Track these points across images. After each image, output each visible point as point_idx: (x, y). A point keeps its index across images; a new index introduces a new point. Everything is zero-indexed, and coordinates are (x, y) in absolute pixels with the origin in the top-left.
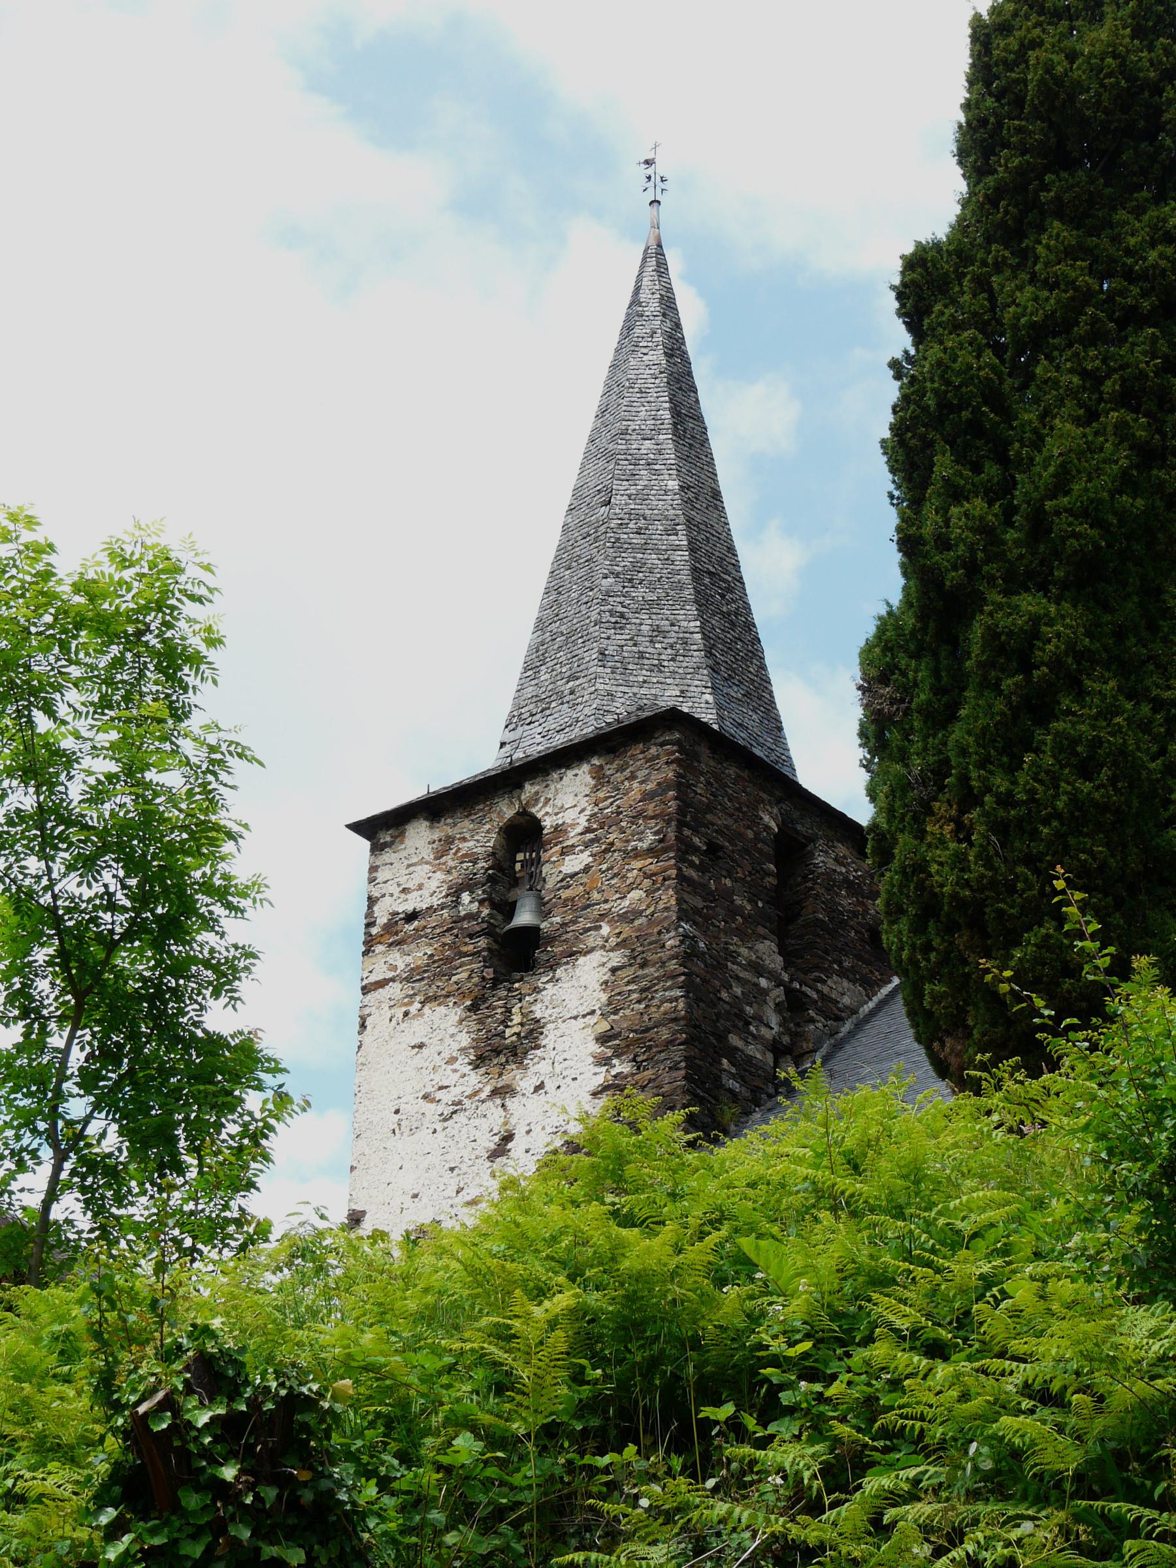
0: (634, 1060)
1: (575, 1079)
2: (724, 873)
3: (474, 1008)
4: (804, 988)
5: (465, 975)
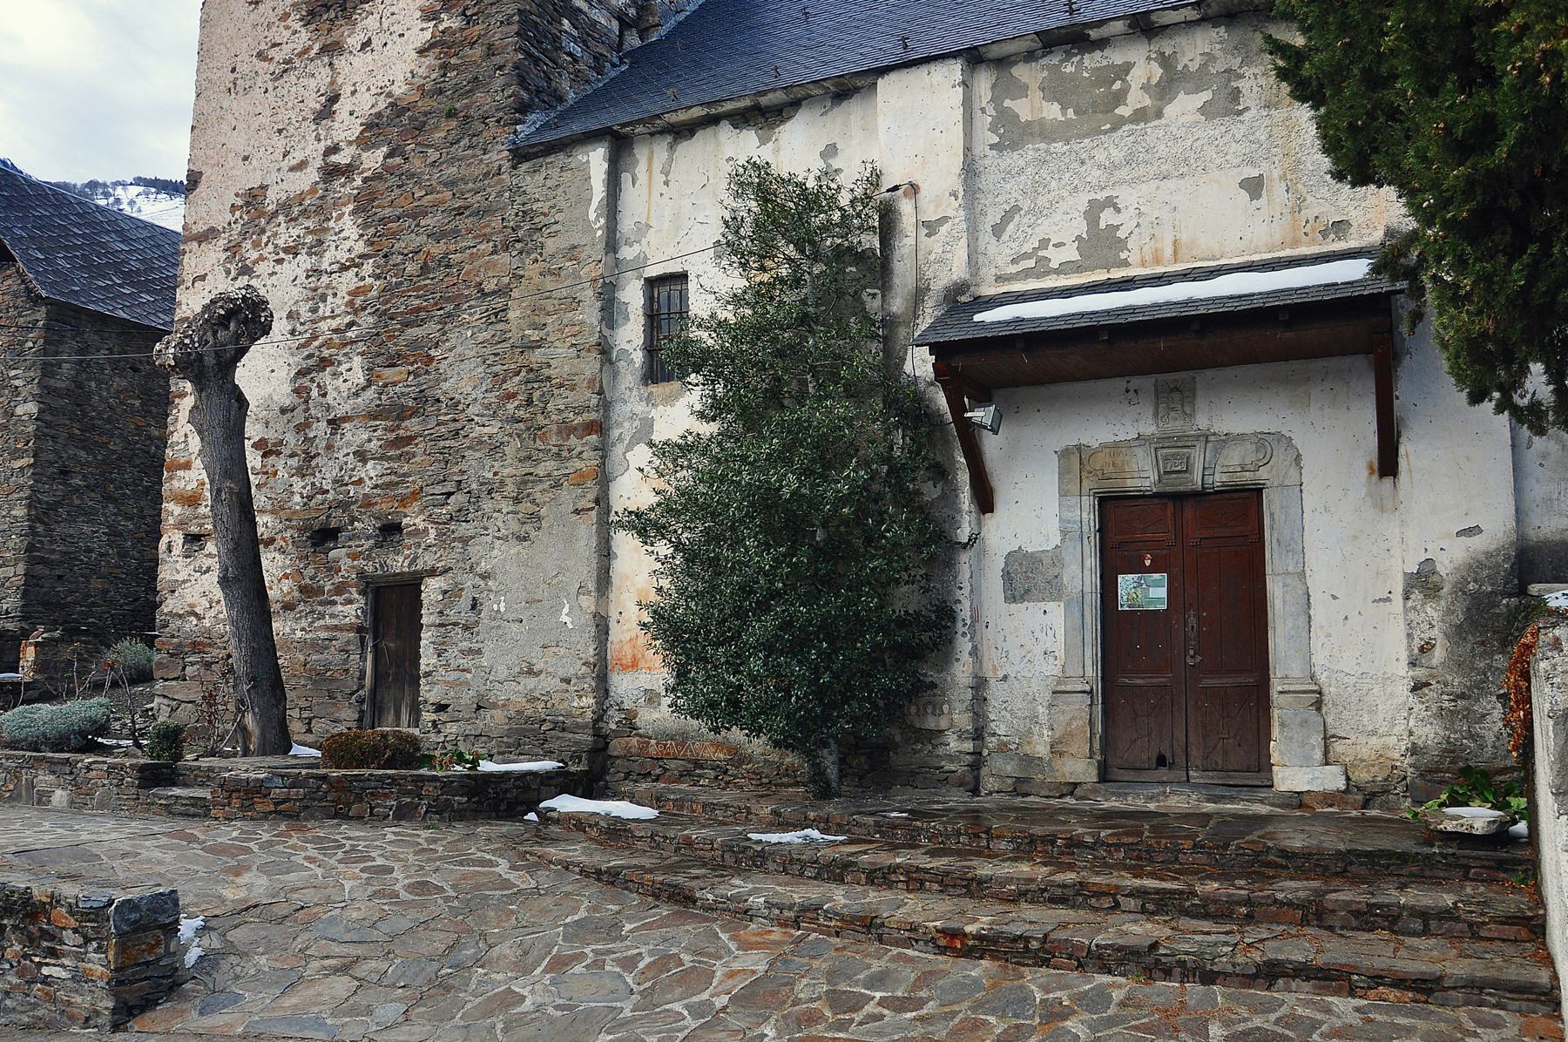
0: (464, 14)
1: (402, 35)
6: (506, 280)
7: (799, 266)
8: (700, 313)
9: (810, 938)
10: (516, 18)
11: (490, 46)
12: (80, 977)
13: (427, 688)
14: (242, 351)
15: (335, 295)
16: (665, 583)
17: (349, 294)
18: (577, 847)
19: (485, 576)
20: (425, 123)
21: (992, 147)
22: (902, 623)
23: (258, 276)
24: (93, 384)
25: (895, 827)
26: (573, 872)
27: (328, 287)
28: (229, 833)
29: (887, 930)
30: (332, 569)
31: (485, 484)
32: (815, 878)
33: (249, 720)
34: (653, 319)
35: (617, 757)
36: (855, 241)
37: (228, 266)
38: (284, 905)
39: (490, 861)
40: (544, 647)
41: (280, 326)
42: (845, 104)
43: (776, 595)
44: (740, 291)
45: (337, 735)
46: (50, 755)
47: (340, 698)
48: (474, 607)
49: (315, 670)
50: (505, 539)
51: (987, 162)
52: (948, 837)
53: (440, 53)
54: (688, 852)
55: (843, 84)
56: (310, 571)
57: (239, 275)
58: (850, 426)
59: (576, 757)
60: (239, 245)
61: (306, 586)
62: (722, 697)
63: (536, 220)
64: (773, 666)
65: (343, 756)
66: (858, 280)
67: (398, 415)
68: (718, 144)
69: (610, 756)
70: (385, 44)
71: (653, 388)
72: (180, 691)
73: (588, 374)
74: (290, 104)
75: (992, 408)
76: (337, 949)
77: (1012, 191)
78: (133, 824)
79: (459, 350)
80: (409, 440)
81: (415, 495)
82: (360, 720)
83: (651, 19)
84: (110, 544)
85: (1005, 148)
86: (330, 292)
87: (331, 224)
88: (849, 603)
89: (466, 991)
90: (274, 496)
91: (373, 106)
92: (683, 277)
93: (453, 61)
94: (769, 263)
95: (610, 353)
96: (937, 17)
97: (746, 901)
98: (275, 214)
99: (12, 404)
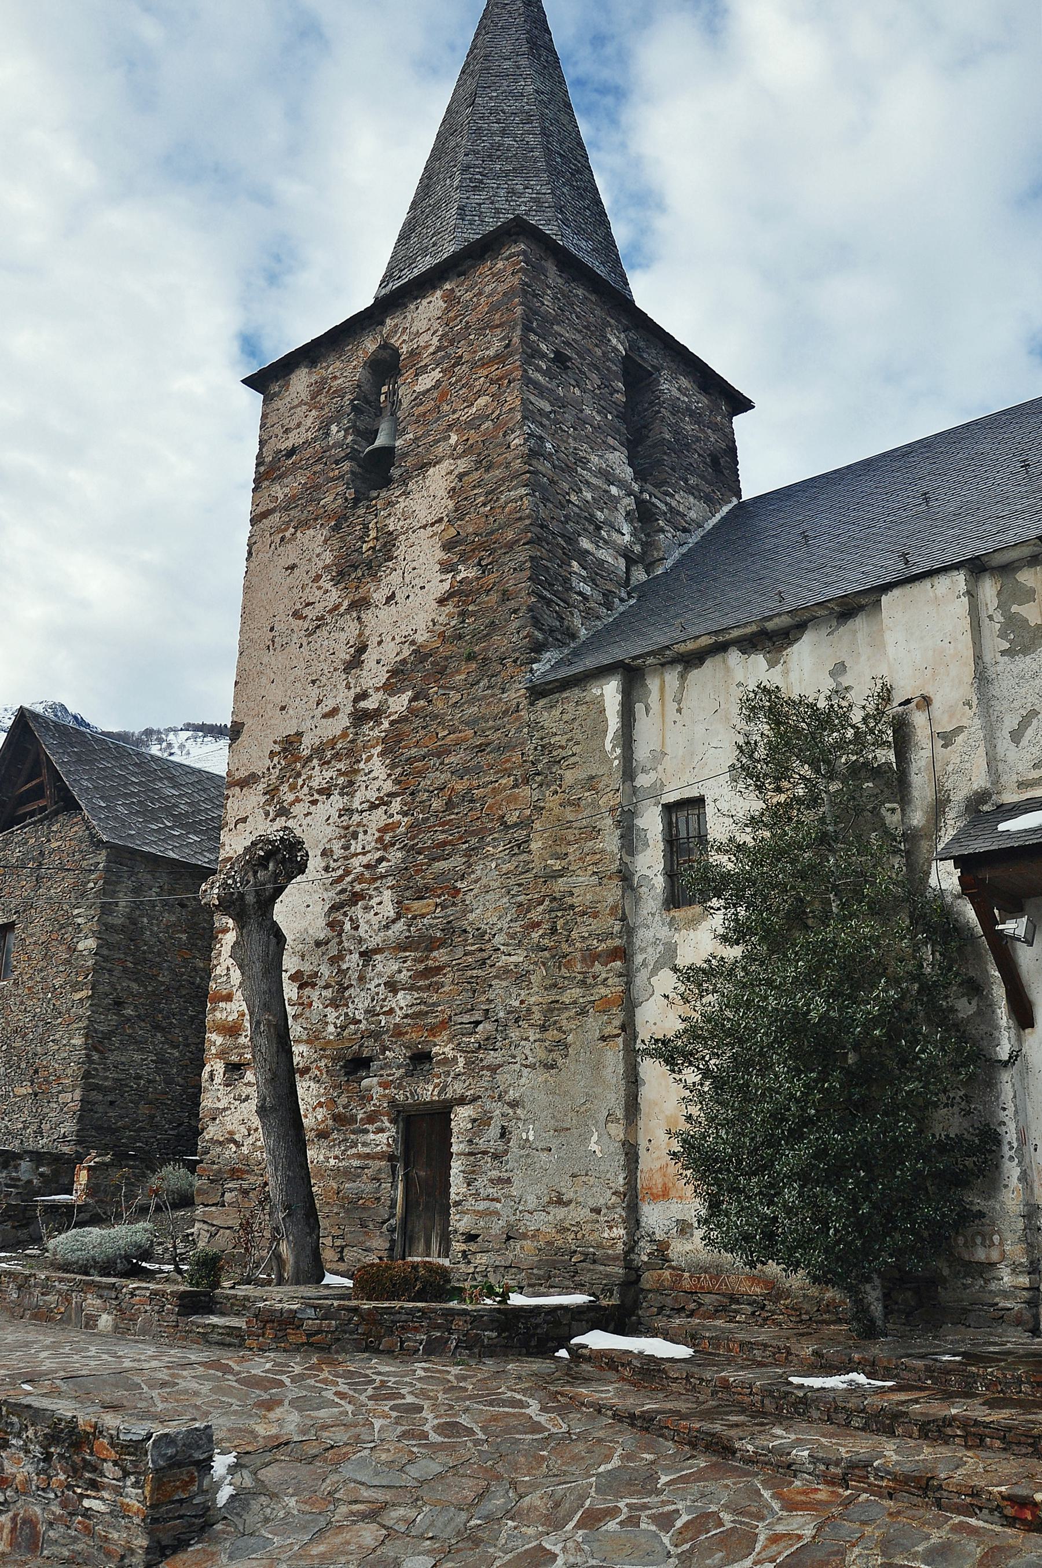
0: (479, 564)
1: (423, 588)
2: (573, 382)
3: (337, 528)
4: (654, 500)
5: (331, 498)
6: (528, 812)
7: (814, 786)
8: (718, 837)
9: (860, 1499)
10: (528, 564)
11: (505, 592)
12: (120, 1512)
13: (457, 1217)
14: (279, 891)
15: (365, 832)
16: (694, 1110)
17: (379, 830)
18: (610, 1388)
19: (514, 1104)
20: (446, 667)
21: (1003, 653)
22: (943, 1147)
23: (295, 817)
24: (145, 920)
25: (948, 1373)
26: (606, 1415)
27: (359, 825)
28: (261, 1366)
29: (945, 1494)
30: (365, 1098)
31: (512, 1012)
32: (863, 1429)
33: (284, 1248)
34: (672, 843)
35: (650, 1291)
36: (870, 757)
37: (268, 808)
38: (314, 1443)
39: (521, 1401)
40: (574, 1176)
41: (315, 863)
42: (850, 622)
43: (809, 1122)
44: (757, 813)
45: (369, 1265)
46: (98, 1279)
47: (371, 1227)
48: (503, 1135)
49: (347, 1198)
50: (532, 1067)
51: (999, 668)
52: (1008, 1385)
53: (459, 601)
54: (725, 1396)
55: (847, 604)
56: (343, 1100)
57: (277, 816)
58: (878, 946)
59: (608, 1291)
60: (277, 789)
61: (339, 1115)
62: (756, 1230)
63: (555, 753)
64: (809, 1196)
65: (374, 1288)
66: (876, 796)
67: (427, 946)
68: (728, 670)
69: (643, 1290)
70: (408, 597)
71: (675, 913)
72: (220, 1217)
73: (610, 901)
74: (322, 657)
75: (1025, 919)
76: (365, 1493)
77: (1027, 696)
78: (172, 1352)
79: (484, 881)
80: (438, 969)
81: (444, 1024)
82: (391, 1249)
83: (655, 554)
84: (157, 1071)
85: (1017, 653)
86: (361, 829)
87: (362, 765)
88: (885, 1129)
89: (495, 1546)
90: (309, 1026)
91: (398, 654)
92: (699, 802)
93: (470, 608)
94: (785, 784)
95: (632, 880)
96: (936, 530)
97: (789, 1454)
98: (309, 759)
99: (75, 940)
